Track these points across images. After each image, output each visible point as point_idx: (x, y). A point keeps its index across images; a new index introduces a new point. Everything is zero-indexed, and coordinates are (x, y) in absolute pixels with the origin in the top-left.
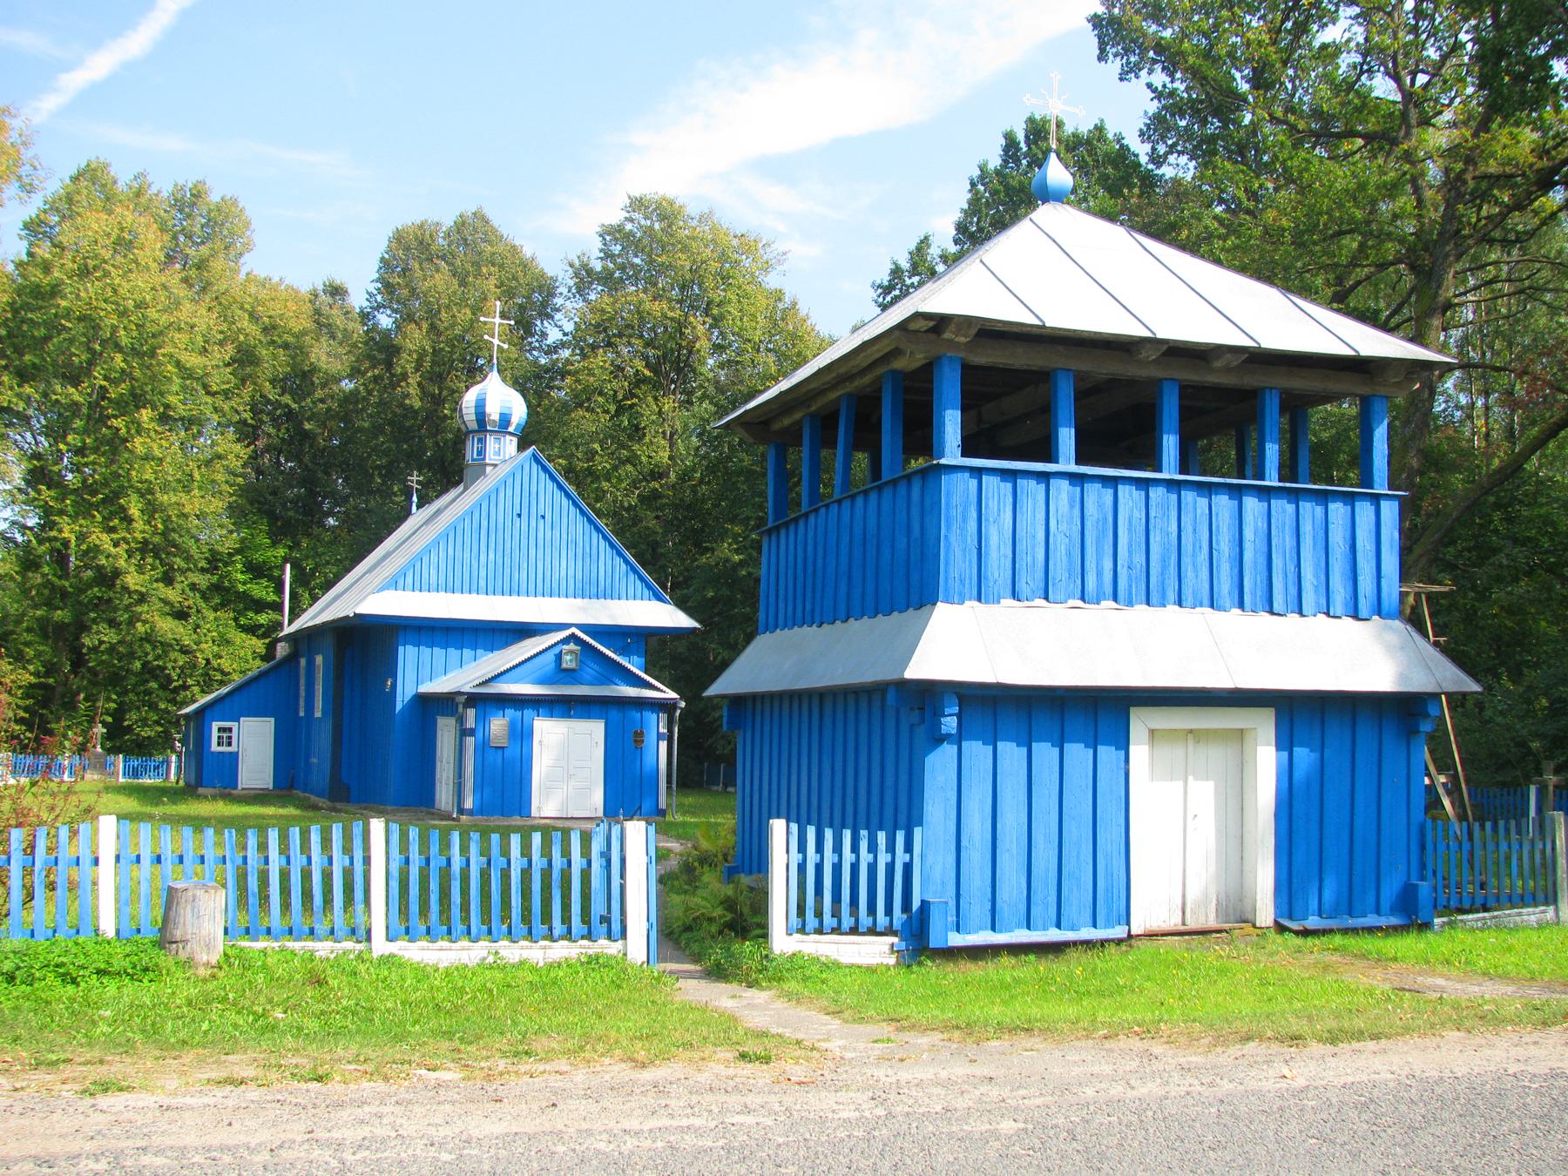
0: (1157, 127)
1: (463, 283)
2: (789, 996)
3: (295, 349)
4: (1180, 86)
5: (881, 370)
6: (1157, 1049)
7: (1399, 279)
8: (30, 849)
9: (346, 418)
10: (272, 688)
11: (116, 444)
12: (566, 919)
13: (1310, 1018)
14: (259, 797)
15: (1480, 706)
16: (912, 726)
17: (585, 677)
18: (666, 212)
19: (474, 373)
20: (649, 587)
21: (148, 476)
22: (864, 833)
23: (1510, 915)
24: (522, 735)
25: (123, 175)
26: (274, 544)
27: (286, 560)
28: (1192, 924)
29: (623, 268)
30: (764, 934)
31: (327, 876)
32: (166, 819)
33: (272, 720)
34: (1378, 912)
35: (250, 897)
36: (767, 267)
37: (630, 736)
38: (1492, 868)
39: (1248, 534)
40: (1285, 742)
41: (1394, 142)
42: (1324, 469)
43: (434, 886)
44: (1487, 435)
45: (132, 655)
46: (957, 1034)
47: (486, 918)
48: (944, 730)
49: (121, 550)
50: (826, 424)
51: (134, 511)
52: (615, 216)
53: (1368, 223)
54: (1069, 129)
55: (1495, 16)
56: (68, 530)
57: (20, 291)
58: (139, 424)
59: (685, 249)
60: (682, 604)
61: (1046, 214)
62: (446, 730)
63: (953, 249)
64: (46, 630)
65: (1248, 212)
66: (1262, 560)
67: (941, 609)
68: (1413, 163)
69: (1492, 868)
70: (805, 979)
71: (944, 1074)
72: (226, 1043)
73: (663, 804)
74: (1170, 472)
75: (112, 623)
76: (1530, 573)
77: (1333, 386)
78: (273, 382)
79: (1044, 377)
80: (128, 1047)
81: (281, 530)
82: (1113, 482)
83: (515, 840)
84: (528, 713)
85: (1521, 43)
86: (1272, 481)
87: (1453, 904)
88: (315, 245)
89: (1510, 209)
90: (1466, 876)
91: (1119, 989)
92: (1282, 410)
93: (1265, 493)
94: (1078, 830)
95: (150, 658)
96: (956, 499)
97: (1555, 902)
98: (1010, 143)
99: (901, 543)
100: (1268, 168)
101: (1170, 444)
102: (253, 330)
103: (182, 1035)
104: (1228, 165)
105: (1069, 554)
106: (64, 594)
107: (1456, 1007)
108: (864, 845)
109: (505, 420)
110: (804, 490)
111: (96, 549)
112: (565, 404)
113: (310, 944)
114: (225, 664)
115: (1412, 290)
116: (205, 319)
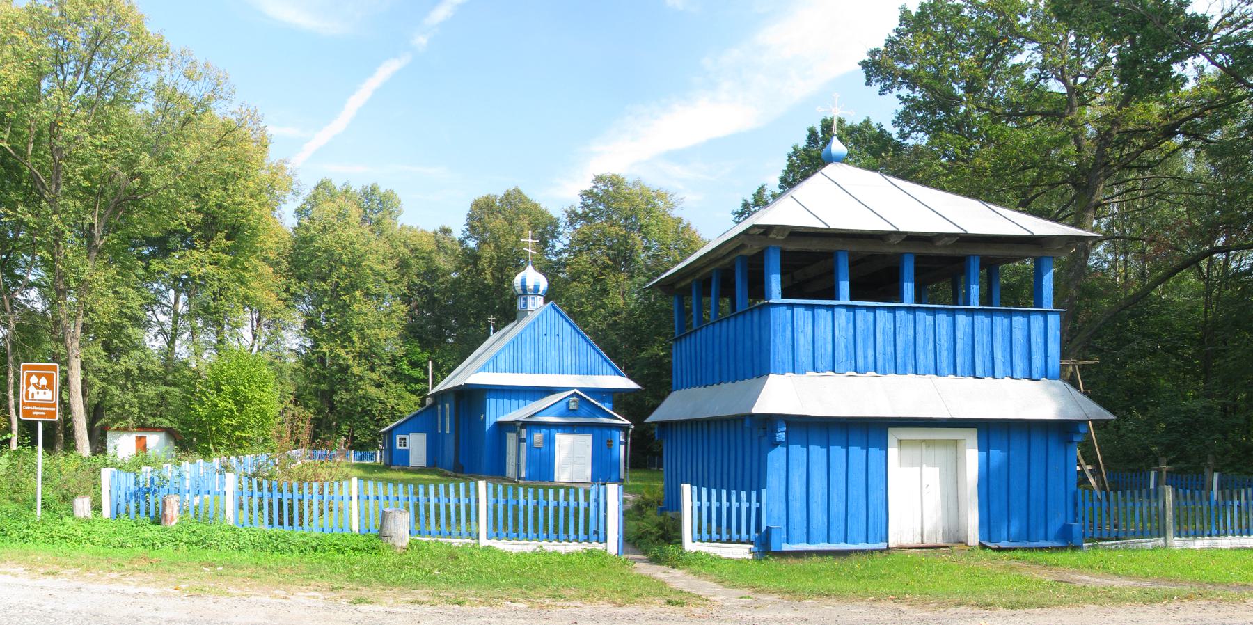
0: (903, 119)
1: (511, 223)
2: (694, 573)
3: (428, 259)
4: (918, 95)
5: (735, 255)
6: (904, 608)
7: (1077, 191)
8: (321, 492)
9: (455, 291)
10: (425, 419)
11: (345, 308)
12: (576, 531)
13: (999, 595)
14: (420, 470)
15: (1118, 427)
16: (759, 438)
17: (583, 413)
18: (615, 182)
19: (519, 267)
22: (733, 492)
23: (1135, 543)
24: (550, 441)
25: (338, 184)
26: (422, 352)
27: (429, 359)
28: (927, 543)
29: (593, 211)
30: (680, 541)
31: (458, 508)
32: (376, 480)
34: (1046, 539)
35: (421, 517)
36: (672, 206)
37: (605, 444)
38: (1122, 516)
39: (959, 335)
40: (984, 446)
41: (1062, 116)
42: (1012, 297)
43: (510, 514)
44: (1126, 276)
45: (356, 405)
46: (787, 596)
47: (556, 531)
48: (778, 439)
49: (350, 356)
50: (705, 285)
51: (355, 338)
52: (588, 186)
53: (1044, 162)
54: (848, 123)
55: (1132, 41)
56: (325, 348)
57: (295, 241)
59: (627, 199)
60: (631, 377)
61: (830, 169)
62: (511, 440)
63: (779, 191)
64: (318, 394)
65: (963, 160)
66: (968, 349)
67: (772, 378)
68: (1075, 127)
69: (1122, 516)
70: (703, 565)
71: (779, 616)
72: (413, 584)
73: (622, 476)
74: (909, 301)
75: (347, 390)
76: (1155, 352)
77: (1016, 253)
78: (417, 275)
79: (831, 255)
80: (369, 584)
81: (425, 345)
82: (873, 309)
83: (551, 492)
84: (553, 431)
85: (1149, 56)
86: (975, 305)
87: (1095, 536)
88: (435, 209)
89: (1143, 149)
90: (1105, 521)
91: (882, 576)
92: (981, 268)
93: (971, 313)
94: (857, 492)
96: (779, 321)
97: (1165, 535)
98: (812, 134)
99: (748, 344)
100: (977, 136)
101: (909, 288)
102: (407, 251)
103: (393, 579)
104: (950, 136)
105: (846, 347)
106: (325, 377)
107: (1094, 591)
108: (733, 498)
109: (537, 289)
110: (694, 321)
111: (338, 356)
112: (566, 280)
113: (449, 540)
114: (401, 408)
115: (1074, 198)
116: (383, 248)
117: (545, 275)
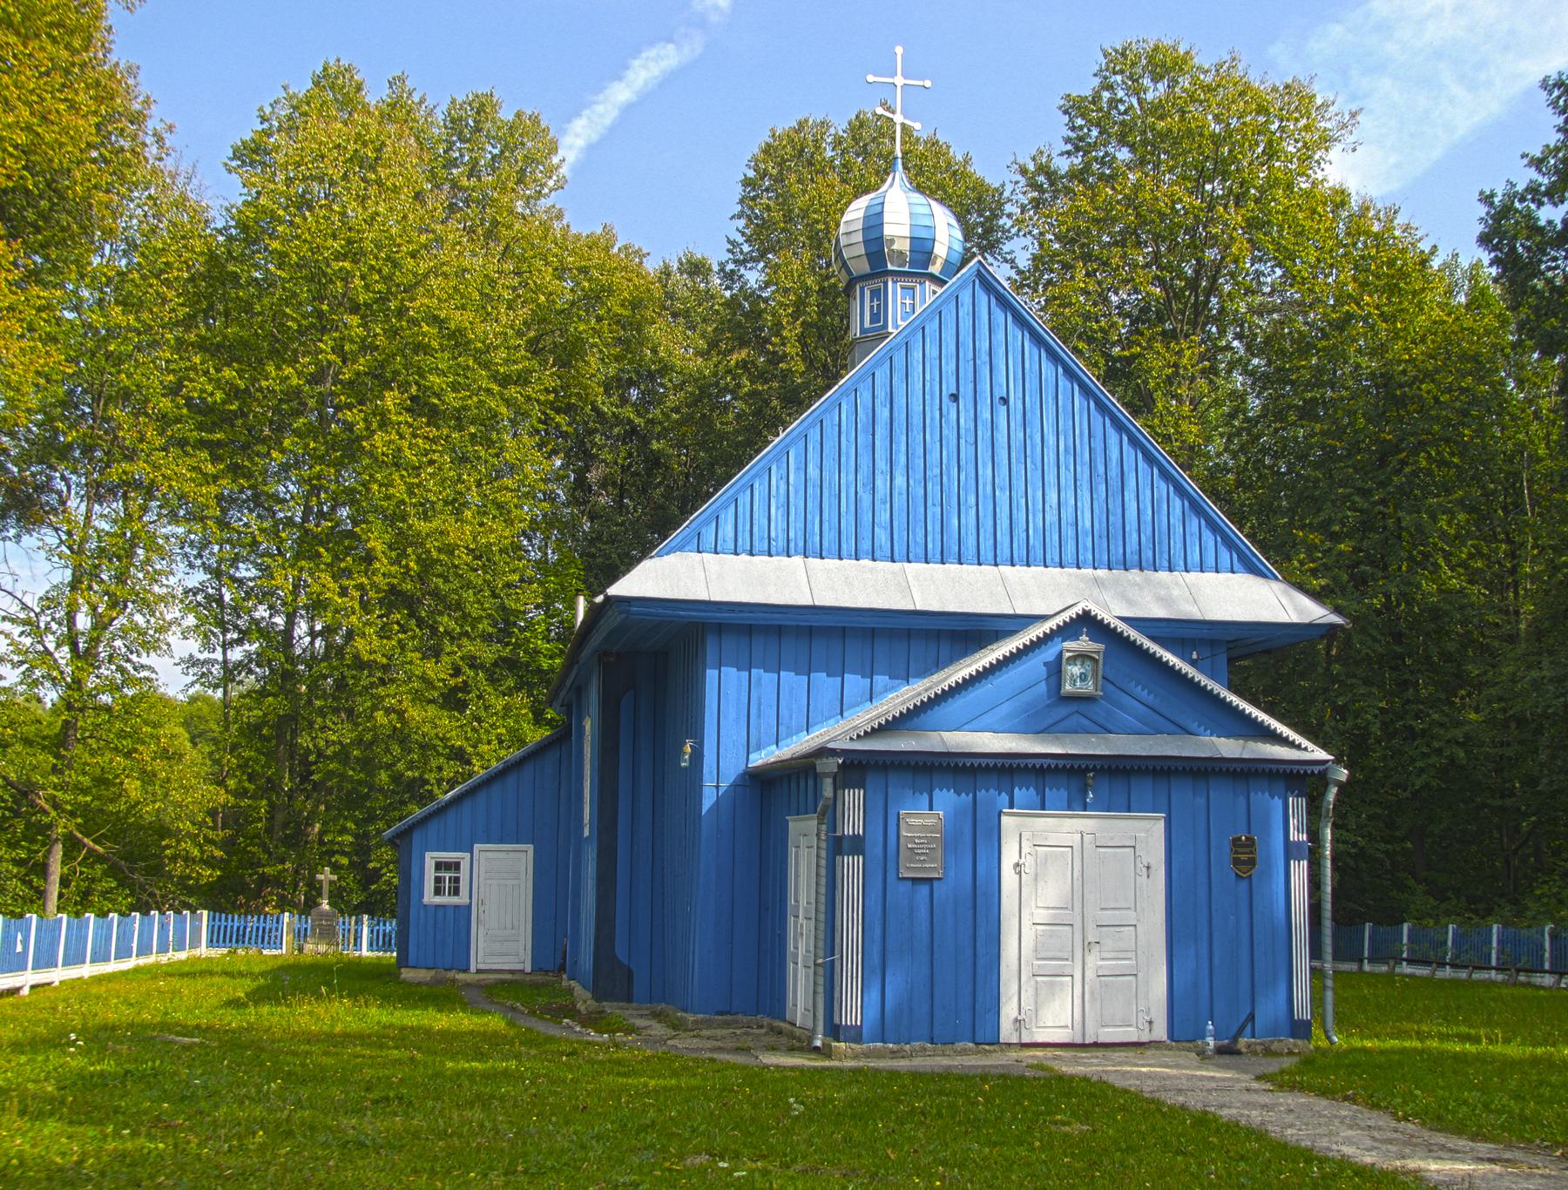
17: (1127, 722)
20: (1230, 544)
21: (399, 491)
24: (980, 839)
33: (530, 848)
37: (1223, 855)
51: (376, 545)
58: (383, 415)
95: (401, 766)
117: (961, 218)
